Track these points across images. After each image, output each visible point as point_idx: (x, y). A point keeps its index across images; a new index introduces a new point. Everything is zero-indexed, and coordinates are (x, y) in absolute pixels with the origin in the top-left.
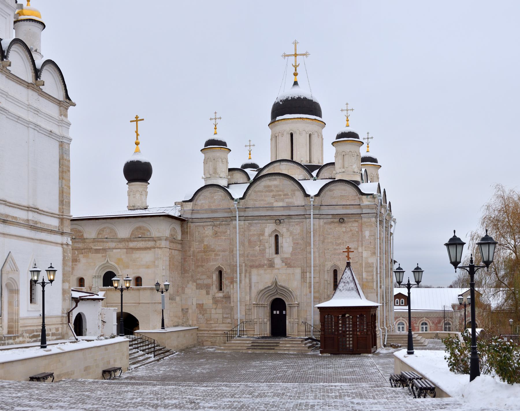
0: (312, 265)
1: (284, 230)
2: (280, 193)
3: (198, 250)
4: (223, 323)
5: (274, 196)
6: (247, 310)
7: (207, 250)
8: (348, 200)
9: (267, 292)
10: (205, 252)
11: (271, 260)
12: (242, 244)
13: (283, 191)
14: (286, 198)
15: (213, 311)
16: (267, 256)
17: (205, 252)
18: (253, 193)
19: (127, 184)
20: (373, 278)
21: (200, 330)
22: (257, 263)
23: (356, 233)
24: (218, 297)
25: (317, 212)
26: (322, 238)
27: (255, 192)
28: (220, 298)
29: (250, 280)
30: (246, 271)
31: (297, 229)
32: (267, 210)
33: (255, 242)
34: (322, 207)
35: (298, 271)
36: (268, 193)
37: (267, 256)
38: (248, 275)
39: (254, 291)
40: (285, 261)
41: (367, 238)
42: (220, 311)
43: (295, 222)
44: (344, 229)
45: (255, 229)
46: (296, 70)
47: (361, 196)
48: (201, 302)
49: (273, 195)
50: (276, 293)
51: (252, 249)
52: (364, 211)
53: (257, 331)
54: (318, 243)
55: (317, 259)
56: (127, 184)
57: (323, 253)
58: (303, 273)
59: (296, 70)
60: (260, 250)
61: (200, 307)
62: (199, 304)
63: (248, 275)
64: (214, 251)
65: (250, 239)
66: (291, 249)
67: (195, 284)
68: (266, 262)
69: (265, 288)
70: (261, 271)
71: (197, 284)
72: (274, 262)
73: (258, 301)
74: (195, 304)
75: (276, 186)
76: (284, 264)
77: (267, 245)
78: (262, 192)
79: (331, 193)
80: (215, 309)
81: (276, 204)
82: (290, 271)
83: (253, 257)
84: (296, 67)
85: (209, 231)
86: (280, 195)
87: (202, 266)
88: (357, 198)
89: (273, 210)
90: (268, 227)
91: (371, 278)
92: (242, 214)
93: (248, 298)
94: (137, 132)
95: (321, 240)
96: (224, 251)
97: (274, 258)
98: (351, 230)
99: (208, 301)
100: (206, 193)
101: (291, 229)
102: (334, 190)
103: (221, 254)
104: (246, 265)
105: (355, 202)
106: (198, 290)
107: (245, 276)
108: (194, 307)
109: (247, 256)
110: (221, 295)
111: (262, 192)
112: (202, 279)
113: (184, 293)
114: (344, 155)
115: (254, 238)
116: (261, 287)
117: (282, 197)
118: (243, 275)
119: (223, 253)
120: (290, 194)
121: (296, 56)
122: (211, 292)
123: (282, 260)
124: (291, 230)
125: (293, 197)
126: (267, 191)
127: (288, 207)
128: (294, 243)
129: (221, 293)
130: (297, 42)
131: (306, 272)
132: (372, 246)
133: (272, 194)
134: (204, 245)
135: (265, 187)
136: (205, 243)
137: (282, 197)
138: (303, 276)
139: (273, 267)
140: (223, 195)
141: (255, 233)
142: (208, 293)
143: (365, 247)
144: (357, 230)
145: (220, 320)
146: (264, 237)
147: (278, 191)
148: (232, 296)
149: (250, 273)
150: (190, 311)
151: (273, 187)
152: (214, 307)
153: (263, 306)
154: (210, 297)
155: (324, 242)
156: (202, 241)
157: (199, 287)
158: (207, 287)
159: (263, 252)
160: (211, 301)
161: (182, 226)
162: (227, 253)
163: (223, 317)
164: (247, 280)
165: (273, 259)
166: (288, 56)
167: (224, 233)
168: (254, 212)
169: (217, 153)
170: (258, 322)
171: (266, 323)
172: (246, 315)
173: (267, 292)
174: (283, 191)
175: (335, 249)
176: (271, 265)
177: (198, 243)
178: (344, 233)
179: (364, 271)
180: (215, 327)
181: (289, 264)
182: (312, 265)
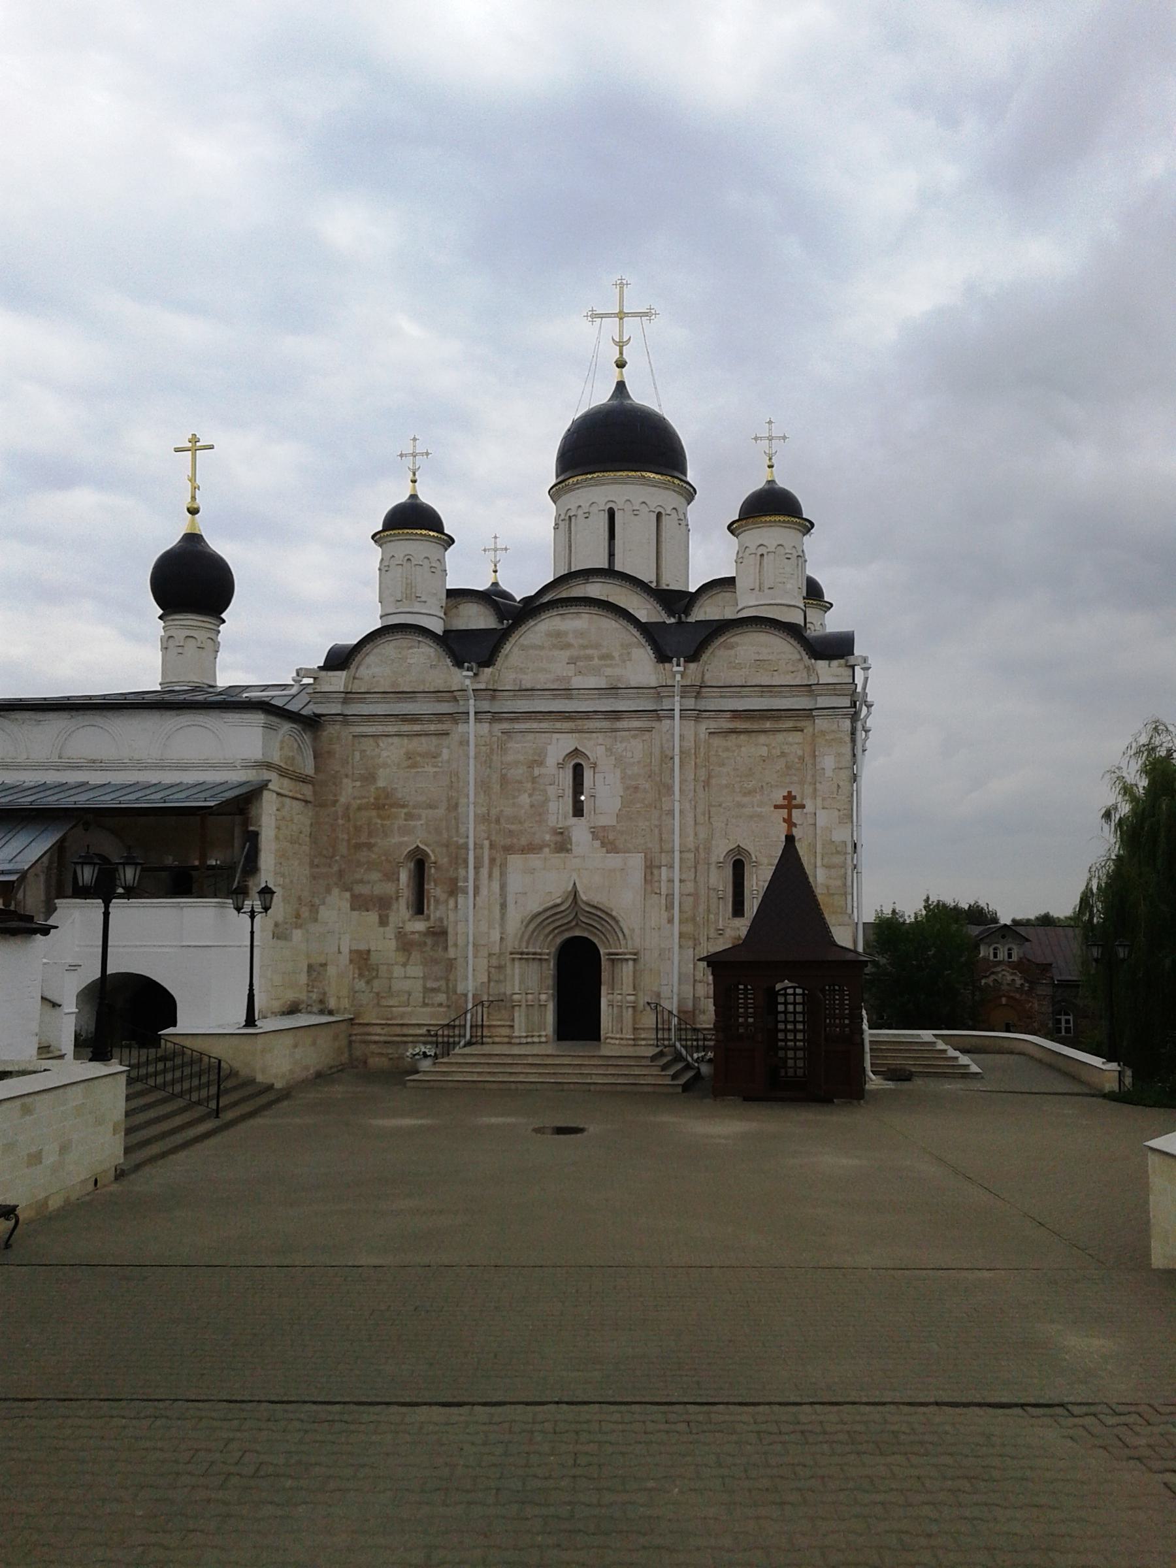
0: (677, 847)
1: (601, 750)
2: (589, 652)
3: (359, 802)
4: (425, 1005)
5: (572, 661)
6: (493, 970)
7: (384, 803)
8: (775, 673)
9: (550, 920)
10: (378, 807)
11: (562, 833)
12: (484, 786)
13: (597, 646)
14: (607, 666)
15: (398, 971)
16: (552, 821)
17: (378, 807)
18: (515, 650)
19: (160, 618)
20: (845, 885)
21: (360, 1024)
22: (524, 841)
23: (797, 760)
24: (413, 933)
25: (690, 703)
26: (703, 773)
27: (523, 648)
28: (417, 936)
29: (503, 887)
30: (492, 861)
31: (634, 748)
32: (555, 697)
33: (520, 782)
34: (704, 690)
35: (636, 861)
36: (556, 653)
37: (552, 821)
38: (496, 872)
39: (515, 918)
40: (601, 835)
41: (829, 773)
42: (415, 970)
43: (629, 730)
44: (764, 751)
45: (519, 748)
46: (621, 353)
47: (813, 661)
48: (363, 947)
49: (571, 658)
50: (574, 923)
51: (511, 801)
52: (822, 702)
53: (520, 1029)
54: (692, 787)
55: (690, 831)
56: (160, 618)
57: (707, 815)
58: (651, 868)
59: (621, 353)
60: (532, 806)
61: (362, 960)
62: (358, 952)
63: (496, 872)
64: (403, 806)
65: (506, 775)
66: (617, 804)
67: (347, 895)
68: (548, 837)
69: (546, 910)
70: (534, 860)
71: (353, 896)
72: (570, 838)
73: (524, 944)
74: (345, 950)
75: (580, 634)
76: (597, 843)
77: (552, 791)
78: (542, 648)
79: (732, 652)
80: (404, 965)
81: (577, 682)
82: (615, 860)
83: (512, 823)
84: (621, 345)
85: (391, 752)
86: (590, 658)
87: (370, 846)
88: (801, 666)
89: (570, 697)
90: (554, 741)
91: (839, 883)
92: (485, 706)
93: (496, 935)
94: (193, 479)
95: (703, 778)
96: (431, 806)
97: (571, 826)
98: (783, 754)
99: (383, 944)
100: (389, 648)
101: (620, 747)
102: (737, 644)
103: (424, 813)
104: (492, 846)
105: (796, 677)
106: (356, 913)
107: (490, 876)
108: (345, 958)
109: (498, 821)
110: (420, 926)
111: (542, 648)
112: (369, 882)
113: (316, 920)
114: (762, 555)
115: (518, 773)
116: (534, 906)
117: (596, 661)
118: (484, 872)
119: (430, 811)
120: (616, 654)
121: (621, 319)
122: (393, 919)
123: (593, 833)
124: (619, 750)
125: (624, 662)
126: (554, 646)
127: (613, 690)
128: (627, 788)
129: (419, 920)
130: (624, 282)
131: (660, 867)
132: (843, 797)
133: (567, 653)
134: (377, 789)
135: (549, 634)
136: (381, 783)
137: (596, 661)
138: (649, 878)
139: (568, 851)
140: (432, 655)
141: (521, 758)
142: (383, 922)
143: (824, 799)
144: (800, 753)
145: (418, 996)
146: (543, 771)
147: (585, 647)
148: (450, 930)
149: (503, 865)
150: (332, 970)
151: (571, 635)
152: (402, 960)
153: (537, 958)
154: (390, 931)
155: (708, 786)
156: (370, 778)
157: (360, 903)
158: (383, 905)
159: (539, 811)
160: (392, 944)
161: (315, 739)
162: (441, 812)
163: (425, 987)
164: (496, 886)
165: (567, 828)
166: (602, 316)
167: (434, 757)
168: (519, 702)
169: (415, 546)
170: (524, 1004)
171: (546, 1005)
172: (489, 981)
173: (550, 920)
174: (597, 646)
175: (740, 805)
176: (563, 844)
177: (358, 784)
178: (764, 761)
179: (819, 863)
180: (402, 1016)
181: (612, 843)
182: (677, 847)
